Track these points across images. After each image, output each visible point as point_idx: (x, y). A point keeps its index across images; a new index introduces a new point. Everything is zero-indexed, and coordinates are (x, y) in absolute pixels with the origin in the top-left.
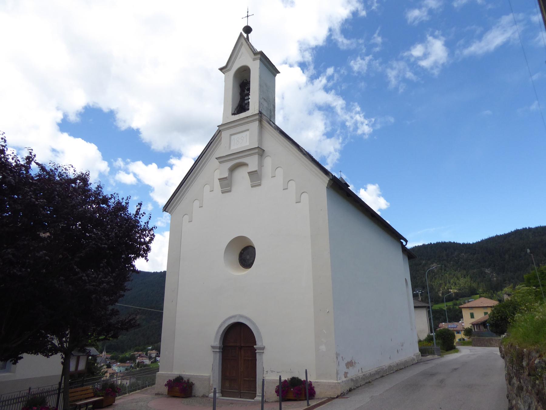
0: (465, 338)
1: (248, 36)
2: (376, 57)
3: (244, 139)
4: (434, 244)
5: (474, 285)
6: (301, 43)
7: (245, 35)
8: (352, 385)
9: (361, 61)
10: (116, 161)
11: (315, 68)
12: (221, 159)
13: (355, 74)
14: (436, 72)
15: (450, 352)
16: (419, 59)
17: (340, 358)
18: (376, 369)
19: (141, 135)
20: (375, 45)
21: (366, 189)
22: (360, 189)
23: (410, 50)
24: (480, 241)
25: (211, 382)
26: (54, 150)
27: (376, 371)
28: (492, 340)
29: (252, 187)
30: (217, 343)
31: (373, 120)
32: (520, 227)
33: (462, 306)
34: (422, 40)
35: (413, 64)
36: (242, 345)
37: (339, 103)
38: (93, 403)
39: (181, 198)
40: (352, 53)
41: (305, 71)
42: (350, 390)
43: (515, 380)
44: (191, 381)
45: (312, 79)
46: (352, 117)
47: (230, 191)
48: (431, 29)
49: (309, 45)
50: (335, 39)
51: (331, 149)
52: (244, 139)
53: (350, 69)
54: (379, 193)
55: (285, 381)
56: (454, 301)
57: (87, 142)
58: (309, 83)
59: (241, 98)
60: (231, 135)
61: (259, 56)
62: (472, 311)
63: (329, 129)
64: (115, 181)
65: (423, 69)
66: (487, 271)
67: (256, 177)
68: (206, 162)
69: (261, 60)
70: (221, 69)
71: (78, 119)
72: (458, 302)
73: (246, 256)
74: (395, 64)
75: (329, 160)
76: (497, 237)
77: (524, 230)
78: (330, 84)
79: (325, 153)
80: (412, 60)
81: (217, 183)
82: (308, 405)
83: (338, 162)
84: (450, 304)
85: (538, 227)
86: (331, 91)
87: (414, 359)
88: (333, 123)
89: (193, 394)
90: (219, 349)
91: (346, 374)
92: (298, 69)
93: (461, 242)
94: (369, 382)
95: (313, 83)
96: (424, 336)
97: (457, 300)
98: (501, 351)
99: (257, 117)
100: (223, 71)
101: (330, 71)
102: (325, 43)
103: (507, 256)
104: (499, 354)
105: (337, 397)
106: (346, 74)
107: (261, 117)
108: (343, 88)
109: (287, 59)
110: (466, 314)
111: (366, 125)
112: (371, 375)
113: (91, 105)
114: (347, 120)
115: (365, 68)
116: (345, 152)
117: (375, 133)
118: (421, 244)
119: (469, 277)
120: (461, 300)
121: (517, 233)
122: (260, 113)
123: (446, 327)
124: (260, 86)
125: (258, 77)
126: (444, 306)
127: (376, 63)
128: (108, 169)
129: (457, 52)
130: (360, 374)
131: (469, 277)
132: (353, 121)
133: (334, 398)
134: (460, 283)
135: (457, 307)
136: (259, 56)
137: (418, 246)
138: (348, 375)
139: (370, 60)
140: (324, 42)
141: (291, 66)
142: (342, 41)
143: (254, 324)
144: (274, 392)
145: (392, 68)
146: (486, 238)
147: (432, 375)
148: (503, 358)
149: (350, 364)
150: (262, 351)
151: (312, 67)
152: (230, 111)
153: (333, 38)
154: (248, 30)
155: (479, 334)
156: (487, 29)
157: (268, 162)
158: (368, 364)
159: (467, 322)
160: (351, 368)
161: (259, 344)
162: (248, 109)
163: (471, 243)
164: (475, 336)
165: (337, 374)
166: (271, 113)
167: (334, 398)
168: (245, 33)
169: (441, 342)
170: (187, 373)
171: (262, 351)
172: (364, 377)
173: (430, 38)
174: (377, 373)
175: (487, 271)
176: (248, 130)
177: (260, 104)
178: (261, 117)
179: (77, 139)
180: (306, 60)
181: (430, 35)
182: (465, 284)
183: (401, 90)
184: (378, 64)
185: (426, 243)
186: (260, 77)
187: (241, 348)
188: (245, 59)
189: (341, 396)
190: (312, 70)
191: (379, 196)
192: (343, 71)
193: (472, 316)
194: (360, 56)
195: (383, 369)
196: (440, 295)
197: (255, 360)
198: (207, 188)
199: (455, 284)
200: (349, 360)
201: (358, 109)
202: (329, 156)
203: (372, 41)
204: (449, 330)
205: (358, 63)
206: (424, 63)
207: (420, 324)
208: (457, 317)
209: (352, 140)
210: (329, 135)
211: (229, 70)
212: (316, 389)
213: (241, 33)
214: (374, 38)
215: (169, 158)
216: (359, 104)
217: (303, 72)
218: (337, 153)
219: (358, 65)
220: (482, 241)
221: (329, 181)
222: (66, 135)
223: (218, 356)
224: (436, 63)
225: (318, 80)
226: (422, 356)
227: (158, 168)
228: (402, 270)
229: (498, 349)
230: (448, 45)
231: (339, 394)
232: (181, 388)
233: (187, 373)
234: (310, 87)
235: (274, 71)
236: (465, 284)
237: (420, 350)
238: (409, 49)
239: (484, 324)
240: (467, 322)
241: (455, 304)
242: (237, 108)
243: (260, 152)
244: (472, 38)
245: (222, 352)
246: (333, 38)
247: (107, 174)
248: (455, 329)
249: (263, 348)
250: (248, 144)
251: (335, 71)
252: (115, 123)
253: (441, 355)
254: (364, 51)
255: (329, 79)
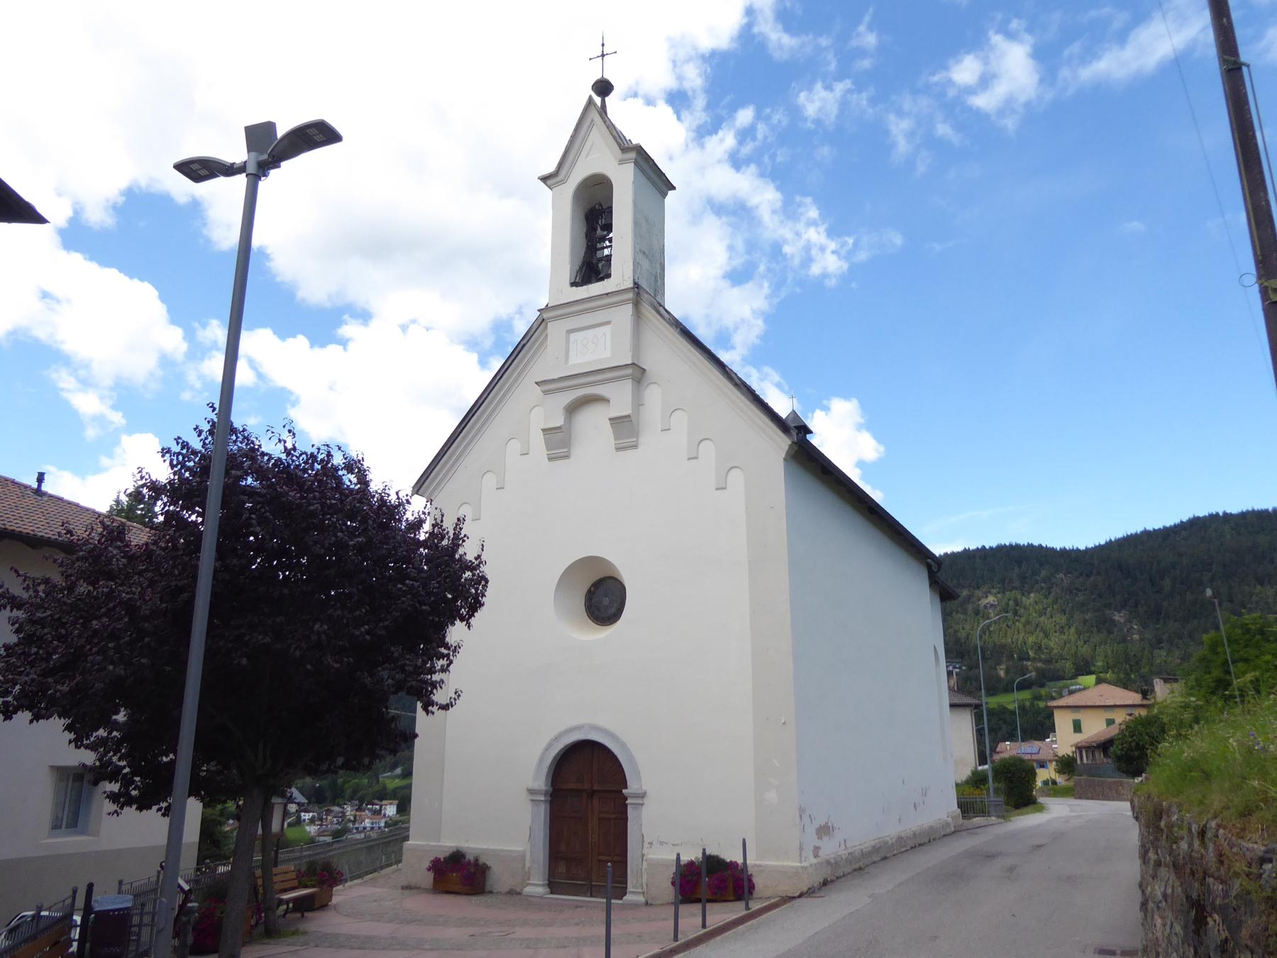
0: (1058, 780)
1: (603, 102)
2: (859, 87)
3: (598, 344)
4: (991, 548)
5: (1085, 650)
6: (674, 44)
7: (598, 100)
8: (827, 873)
9: (824, 94)
10: (204, 326)
11: (709, 107)
12: (548, 386)
13: (810, 125)
14: (1010, 123)
15: (1025, 809)
16: (970, 90)
17: (806, 819)
18: (873, 843)
19: (272, 264)
20: (861, 53)
21: (826, 409)
22: (813, 412)
23: (947, 69)
24: (1103, 542)
25: (528, 865)
26: (45, 295)
27: (874, 847)
28: (1121, 784)
29: (618, 449)
30: (541, 783)
31: (851, 241)
32: (1202, 513)
33: (1055, 703)
34: (976, 43)
35: (954, 105)
36: (595, 788)
37: (765, 197)
38: (295, 900)
39: (453, 465)
40: (803, 71)
41: (685, 114)
42: (825, 883)
43: (1152, 855)
44: (482, 861)
45: (702, 133)
46: (798, 234)
47: (566, 457)
48: (999, 16)
49: (695, 48)
50: (760, 34)
51: (746, 311)
52: (598, 344)
53: (795, 112)
54: (862, 421)
55: (691, 864)
56: (1035, 689)
57: (131, 278)
58: (691, 145)
59: (588, 247)
60: (570, 332)
61: (633, 155)
62: (1077, 716)
63: (738, 262)
64: (201, 377)
65: (979, 115)
66: (1118, 617)
67: (626, 429)
68: (512, 385)
69: (636, 163)
70: (544, 179)
71: (110, 221)
72: (1043, 692)
73: (603, 598)
74: (907, 104)
75: (738, 339)
76: (1146, 533)
77: (1214, 517)
78: (747, 149)
79: (729, 322)
80: (952, 93)
81: (538, 440)
82: (747, 908)
83: (758, 342)
84: (1025, 695)
85: (1248, 512)
86: (748, 166)
87: (948, 825)
88: (751, 246)
89: (488, 888)
90: (545, 795)
91: (817, 849)
92: (665, 111)
93: (1057, 545)
94: (860, 869)
95: (702, 146)
96: (965, 773)
97: (1042, 686)
98: (1133, 808)
99: (630, 295)
100: (549, 182)
101: (745, 116)
102: (734, 45)
103: (1167, 583)
104: (1130, 813)
105: (800, 896)
106: (785, 123)
107: (638, 294)
108: (779, 159)
109: (637, 83)
110: (1063, 722)
111: (833, 252)
112: (864, 854)
113: (143, 183)
114: (785, 241)
115: (833, 110)
116: (778, 320)
117: (855, 270)
118: (958, 548)
119: (1073, 630)
120: (1052, 687)
121: (1196, 526)
122: (637, 285)
123: (1014, 753)
124: (636, 224)
125: (630, 205)
126: (1011, 701)
127: (862, 99)
128: (184, 347)
129: (1064, 73)
130: (843, 852)
131: (1073, 630)
132: (802, 243)
133: (794, 898)
134: (1052, 644)
135: (1042, 704)
136: (633, 155)
137: (953, 554)
138: (821, 853)
139: (848, 91)
140: (732, 39)
141: (650, 102)
142: (779, 39)
143: (623, 746)
144: (667, 884)
145: (900, 114)
146: (1120, 535)
147: (990, 857)
148: (1137, 818)
149: (824, 830)
150: (639, 801)
151: (700, 102)
152: (566, 273)
153: (755, 30)
154: (603, 88)
155: (1092, 771)
156: (1140, 18)
157: (653, 396)
158: (859, 830)
159: (1064, 740)
160: (825, 838)
161: (632, 787)
162: (609, 276)
163: (1082, 547)
164: (1081, 774)
165: (801, 849)
166: (656, 281)
167: (794, 898)
168: (599, 94)
169: (1016, 788)
170: (473, 844)
171: (639, 801)
172: (851, 858)
173: (997, 39)
174: (876, 850)
175: (1118, 617)
176: (608, 323)
177: (636, 265)
178: (638, 294)
179: (107, 270)
180: (687, 85)
181: (998, 32)
182: (1063, 649)
183: (922, 169)
184: (865, 102)
185: (973, 547)
186: (635, 204)
187: (592, 793)
188: (599, 159)
189: (809, 893)
190: (698, 114)
191: (859, 427)
192: (779, 117)
193: (1077, 727)
194: (823, 81)
195: (886, 843)
196: (1002, 673)
197: (625, 819)
198: (514, 447)
199: (1040, 648)
200: (823, 823)
201: (813, 213)
202: (736, 328)
203: (854, 43)
204: (1022, 761)
205: (816, 97)
206: (982, 101)
207: (954, 747)
208: (1041, 727)
209: (798, 290)
210: (737, 277)
211: (563, 182)
212: (756, 880)
213: (590, 98)
214: (858, 34)
215: (340, 323)
216: (817, 201)
217: (679, 118)
218: (760, 322)
219: (818, 102)
220: (1110, 544)
221: (790, 446)
222: (77, 257)
223: (542, 811)
224: (1009, 102)
225: (715, 138)
226: (964, 817)
227: (312, 346)
228: (919, 621)
229: (1128, 804)
230: (1045, 57)
231: (805, 889)
232: (460, 875)
233: (473, 843)
234: (695, 154)
235: (663, 185)
236: (1063, 649)
237: (960, 805)
238: (945, 67)
239: (1104, 746)
240: (1064, 740)
241: (1038, 698)
242: (581, 268)
243: (637, 374)
244: (1098, 37)
245: (551, 802)
246: (755, 30)
247: (180, 357)
248: (1034, 757)
249: (643, 795)
250: (608, 354)
251: (759, 116)
252: (205, 232)
253: (1004, 817)
254: (833, 67)
255: (745, 134)
